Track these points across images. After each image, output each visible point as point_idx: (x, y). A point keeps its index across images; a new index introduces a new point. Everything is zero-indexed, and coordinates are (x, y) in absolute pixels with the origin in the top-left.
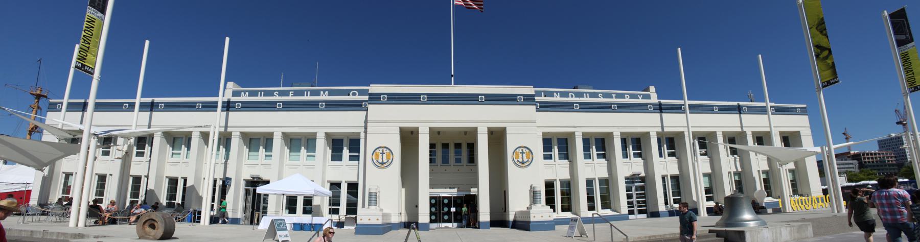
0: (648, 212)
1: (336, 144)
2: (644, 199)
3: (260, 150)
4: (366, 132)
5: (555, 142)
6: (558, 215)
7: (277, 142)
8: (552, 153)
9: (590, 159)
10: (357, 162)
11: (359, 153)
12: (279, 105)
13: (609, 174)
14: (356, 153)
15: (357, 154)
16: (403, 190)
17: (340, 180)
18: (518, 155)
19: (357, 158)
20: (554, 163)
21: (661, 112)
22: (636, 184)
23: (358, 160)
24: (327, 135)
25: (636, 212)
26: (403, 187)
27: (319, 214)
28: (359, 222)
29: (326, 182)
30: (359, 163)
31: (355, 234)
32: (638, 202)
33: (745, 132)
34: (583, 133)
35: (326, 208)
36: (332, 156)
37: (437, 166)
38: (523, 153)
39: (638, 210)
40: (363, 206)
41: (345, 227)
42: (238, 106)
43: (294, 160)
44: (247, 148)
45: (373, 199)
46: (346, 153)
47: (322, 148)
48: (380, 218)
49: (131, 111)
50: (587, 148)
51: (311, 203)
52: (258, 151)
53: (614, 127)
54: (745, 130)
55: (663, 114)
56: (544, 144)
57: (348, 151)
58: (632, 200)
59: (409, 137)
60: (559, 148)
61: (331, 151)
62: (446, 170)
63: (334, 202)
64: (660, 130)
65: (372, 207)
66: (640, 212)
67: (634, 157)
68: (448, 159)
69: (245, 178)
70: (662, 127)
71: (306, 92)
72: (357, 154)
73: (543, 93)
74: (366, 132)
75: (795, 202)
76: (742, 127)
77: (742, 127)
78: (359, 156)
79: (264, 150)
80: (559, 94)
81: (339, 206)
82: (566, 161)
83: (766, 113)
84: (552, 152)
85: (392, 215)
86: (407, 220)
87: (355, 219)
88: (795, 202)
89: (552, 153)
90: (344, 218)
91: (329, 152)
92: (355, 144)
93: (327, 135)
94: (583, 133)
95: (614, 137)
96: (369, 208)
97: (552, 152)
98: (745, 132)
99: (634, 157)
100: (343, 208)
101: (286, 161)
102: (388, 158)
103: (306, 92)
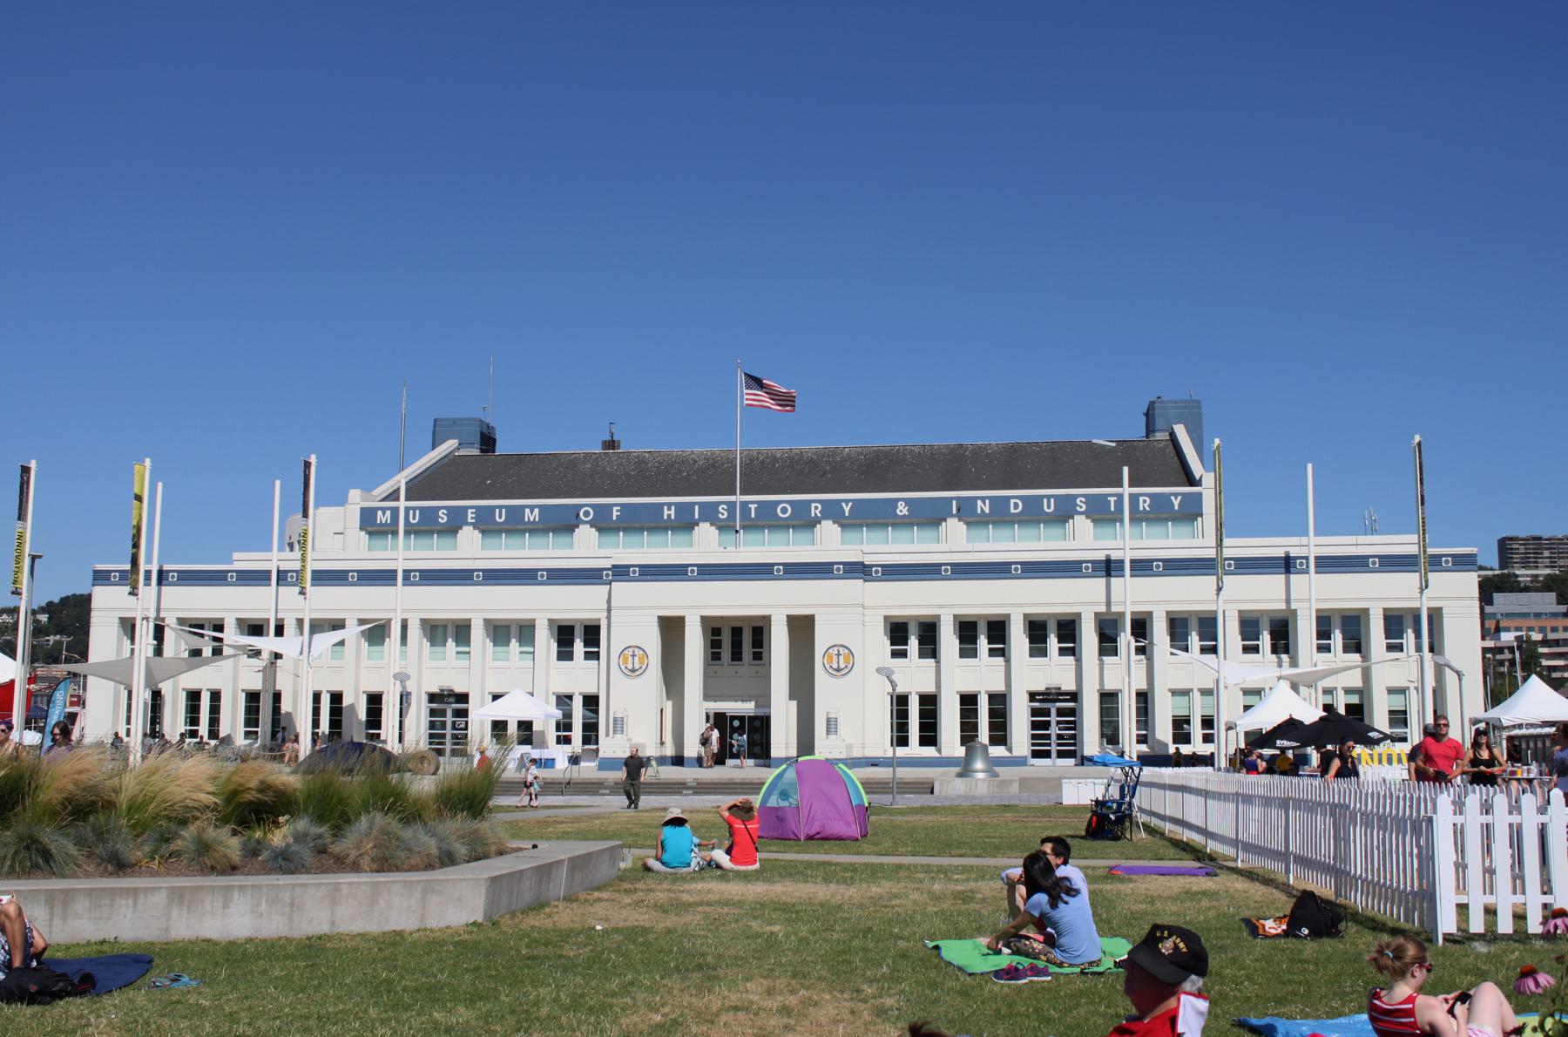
0: (1078, 755)
1: (564, 635)
2: (1073, 732)
3: (447, 644)
4: (609, 618)
5: (1336, 622)
6: (911, 752)
7: (478, 633)
8: (1404, 641)
9: (1117, 655)
10: (596, 662)
11: (599, 647)
12: (542, 576)
13: (1363, 682)
14: (998, 643)
15: (596, 650)
16: (794, 704)
17: (976, 690)
18: (831, 659)
19: (596, 655)
20: (910, 665)
21: (1108, 575)
22: (1059, 705)
23: (598, 659)
24: (487, 622)
25: (1054, 754)
26: (668, 698)
27: (543, 745)
28: (601, 754)
29: (240, 691)
30: (599, 664)
31: (599, 770)
32: (1060, 737)
33: (1295, 611)
34: (1385, 609)
35: (552, 735)
36: (559, 652)
37: (722, 665)
38: (634, 656)
39: (1058, 750)
40: (607, 735)
41: (583, 764)
42: (692, 571)
43: (501, 660)
44: (128, 639)
45: (619, 725)
46: (579, 647)
47: (545, 642)
48: (844, 751)
49: (266, 585)
50: (1324, 633)
51: (532, 728)
52: (444, 644)
53: (941, 606)
54: (1293, 606)
55: (1113, 579)
56: (599, 639)
57: (582, 644)
58: (1049, 732)
59: (671, 628)
60: (1343, 632)
61: (556, 644)
62: (716, 672)
63: (564, 726)
64: (1103, 609)
65: (618, 736)
66: (1061, 755)
67: (1137, 654)
68: (741, 653)
69: (366, 690)
70: (1108, 604)
71: (497, 511)
72: (596, 650)
73: (954, 502)
74: (609, 618)
75: (1372, 759)
76: (1288, 601)
77: (1288, 601)
78: (598, 653)
79: (454, 644)
80: (987, 502)
81: (571, 731)
82: (1143, 657)
83: (1416, 568)
84: (1330, 639)
85: (647, 746)
86: (674, 755)
87: (597, 751)
88: (1372, 759)
89: (1331, 642)
90: (580, 751)
91: (554, 646)
92: (592, 634)
93: (487, 622)
94: (1385, 609)
95: (1444, 616)
96: (613, 737)
97: (1330, 639)
98: (1295, 611)
99: (1137, 654)
100: (577, 734)
101: (490, 663)
102: (641, 662)
103: (497, 511)
